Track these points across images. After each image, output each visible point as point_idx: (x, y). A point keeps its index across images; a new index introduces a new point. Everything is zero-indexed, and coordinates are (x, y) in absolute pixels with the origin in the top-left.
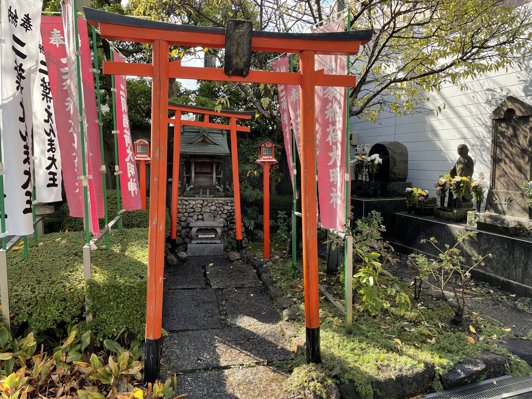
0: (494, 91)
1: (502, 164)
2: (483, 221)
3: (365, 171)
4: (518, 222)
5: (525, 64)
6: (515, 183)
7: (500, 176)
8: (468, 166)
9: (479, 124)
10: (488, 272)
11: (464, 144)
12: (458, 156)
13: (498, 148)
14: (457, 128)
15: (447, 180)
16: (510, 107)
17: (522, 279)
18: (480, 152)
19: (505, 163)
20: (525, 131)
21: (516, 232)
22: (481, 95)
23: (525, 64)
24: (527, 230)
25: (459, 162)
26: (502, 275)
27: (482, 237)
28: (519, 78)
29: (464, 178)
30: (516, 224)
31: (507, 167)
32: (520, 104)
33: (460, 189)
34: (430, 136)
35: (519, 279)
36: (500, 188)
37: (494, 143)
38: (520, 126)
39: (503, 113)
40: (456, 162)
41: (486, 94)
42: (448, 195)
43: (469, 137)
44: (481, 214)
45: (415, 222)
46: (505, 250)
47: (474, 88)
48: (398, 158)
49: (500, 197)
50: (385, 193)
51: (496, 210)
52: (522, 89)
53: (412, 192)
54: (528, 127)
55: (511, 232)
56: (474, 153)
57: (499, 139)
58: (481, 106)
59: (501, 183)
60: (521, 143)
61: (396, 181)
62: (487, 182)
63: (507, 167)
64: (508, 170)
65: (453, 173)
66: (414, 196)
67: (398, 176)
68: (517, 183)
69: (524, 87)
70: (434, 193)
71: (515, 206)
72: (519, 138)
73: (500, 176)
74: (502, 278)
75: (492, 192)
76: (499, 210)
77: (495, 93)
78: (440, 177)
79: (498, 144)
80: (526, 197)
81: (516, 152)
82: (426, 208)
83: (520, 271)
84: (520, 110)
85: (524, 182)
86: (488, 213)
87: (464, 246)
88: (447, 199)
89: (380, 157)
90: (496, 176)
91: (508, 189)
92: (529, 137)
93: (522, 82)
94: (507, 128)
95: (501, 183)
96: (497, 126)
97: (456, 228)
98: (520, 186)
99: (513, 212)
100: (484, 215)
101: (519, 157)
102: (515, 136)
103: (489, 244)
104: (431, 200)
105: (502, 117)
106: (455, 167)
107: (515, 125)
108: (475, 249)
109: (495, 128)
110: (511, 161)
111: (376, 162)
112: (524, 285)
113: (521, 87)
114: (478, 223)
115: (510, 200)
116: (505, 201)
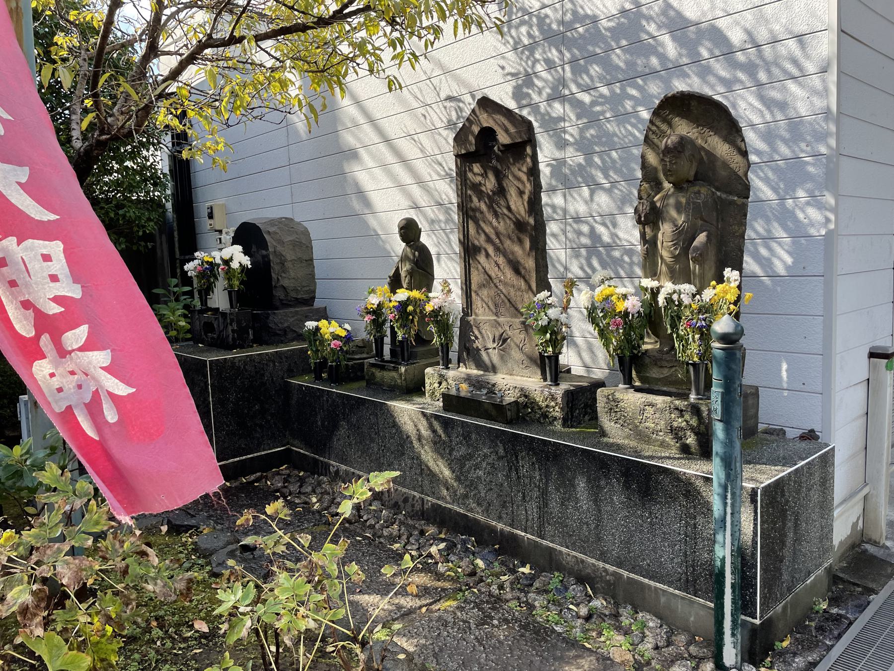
0: (460, 101)
1: (482, 258)
2: (453, 392)
3: (221, 285)
4: (522, 389)
5: (512, 37)
6: (509, 300)
7: (482, 286)
8: (421, 268)
9: (439, 174)
10: (471, 510)
11: (408, 216)
12: (399, 246)
13: (470, 222)
14: (400, 186)
15: (382, 299)
16: (485, 125)
17: (539, 527)
18: (445, 233)
19: (487, 255)
20: (519, 179)
21: (518, 411)
22: (437, 111)
23: (512, 37)
24: (540, 408)
25: (404, 258)
26: (500, 519)
27: (453, 428)
28: (503, 68)
29: (415, 294)
30: (517, 393)
31: (490, 263)
32: (505, 115)
33: (407, 318)
34: (356, 205)
35: (532, 527)
36: (482, 315)
37: (462, 210)
38: (509, 168)
39: (472, 139)
40: (396, 259)
41: (445, 108)
42: (388, 333)
43: (424, 204)
44: (451, 374)
45: (328, 401)
46: (500, 458)
47: (423, 96)
48: (289, 255)
49: (483, 331)
50: (265, 336)
51: (480, 364)
52: (510, 94)
53: (318, 329)
54: (525, 169)
55: (509, 413)
56: (435, 239)
57: (471, 201)
58: (440, 134)
59: (482, 300)
60: (513, 207)
61: (291, 306)
62: (456, 300)
63: (490, 263)
64: (493, 272)
65: (395, 283)
66: (322, 341)
67: (293, 295)
68: (513, 299)
69: (515, 88)
70: (362, 330)
71: (513, 352)
72: (508, 197)
73: (482, 286)
74: (500, 526)
75: (468, 322)
76: (483, 362)
77: (461, 105)
78: (370, 293)
79: (471, 213)
80: (531, 330)
81: (506, 229)
82: (346, 365)
83: (533, 508)
84: (506, 131)
85: (526, 296)
86: (464, 369)
87: (422, 451)
88: (387, 340)
89: (246, 252)
90: (474, 287)
91: (496, 315)
92: (527, 192)
93: (509, 78)
94: (485, 175)
95: (482, 300)
96: (465, 171)
97: (406, 411)
98: (520, 306)
99: (509, 365)
100: (457, 376)
101: (513, 241)
102: (501, 191)
103: (468, 446)
104: (361, 344)
105: (472, 148)
106: (397, 269)
107: (499, 167)
108: (443, 458)
109: (462, 174)
110: (497, 249)
111: (235, 265)
112: (544, 542)
113: (509, 88)
114: (446, 397)
115: (503, 340)
116: (494, 341)
